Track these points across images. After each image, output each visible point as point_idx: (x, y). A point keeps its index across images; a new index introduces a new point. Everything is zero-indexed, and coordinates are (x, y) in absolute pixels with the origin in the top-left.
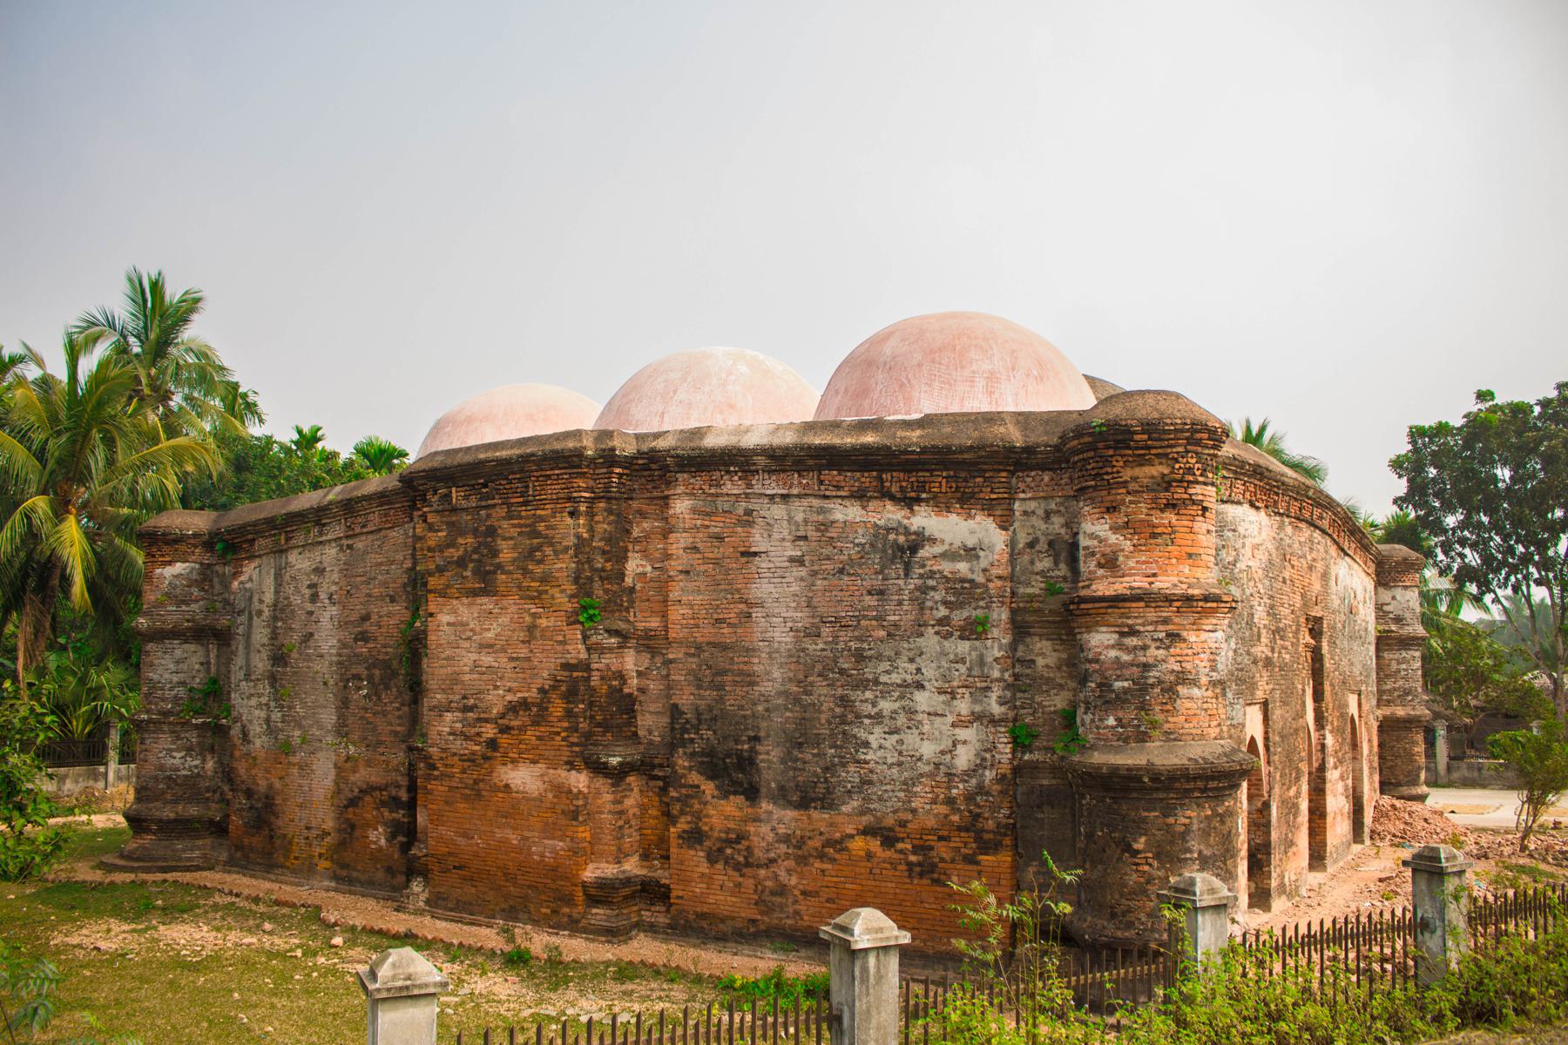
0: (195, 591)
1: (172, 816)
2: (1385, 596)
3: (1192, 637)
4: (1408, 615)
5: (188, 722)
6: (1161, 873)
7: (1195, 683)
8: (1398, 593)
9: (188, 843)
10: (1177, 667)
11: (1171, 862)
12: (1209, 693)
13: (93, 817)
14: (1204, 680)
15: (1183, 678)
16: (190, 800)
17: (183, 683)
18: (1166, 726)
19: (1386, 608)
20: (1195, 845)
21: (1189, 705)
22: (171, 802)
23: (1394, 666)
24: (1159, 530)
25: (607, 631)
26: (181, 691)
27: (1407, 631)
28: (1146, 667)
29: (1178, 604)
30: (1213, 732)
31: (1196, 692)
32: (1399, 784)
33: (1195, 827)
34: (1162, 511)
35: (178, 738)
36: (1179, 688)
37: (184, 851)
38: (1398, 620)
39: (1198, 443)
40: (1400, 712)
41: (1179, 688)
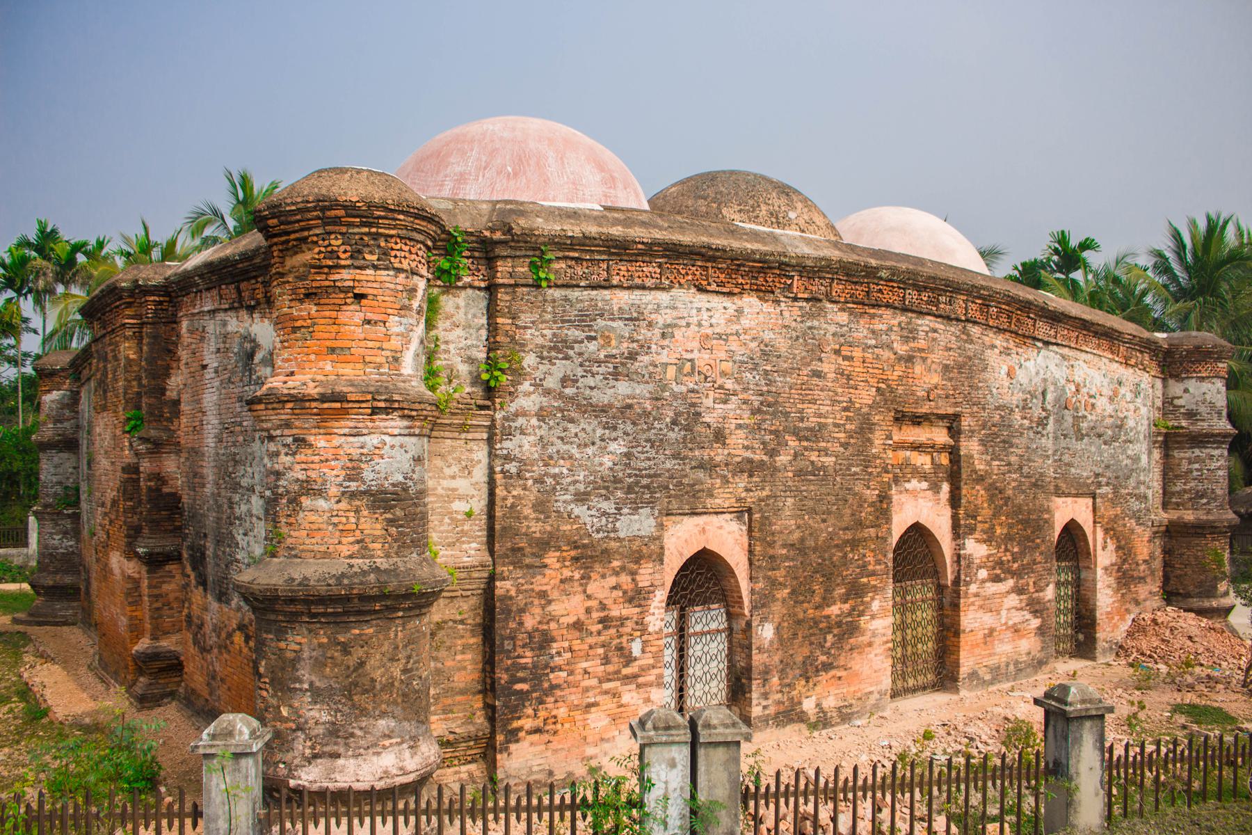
0: (67, 413)
1: (51, 583)
2: (1176, 388)
3: (321, 443)
4: (1203, 409)
5: (60, 513)
6: (274, 702)
7: (320, 493)
8: (1192, 385)
9: (65, 604)
10: (302, 476)
11: (281, 690)
12: (344, 505)
13: (1140, 558)
14: (334, 491)
15: (309, 488)
16: (66, 572)
17: (60, 483)
18: (289, 541)
19: (1177, 402)
20: (306, 674)
21: (314, 518)
22: (53, 573)
23: (1185, 466)
24: (298, 324)
25: (140, 439)
26: (59, 489)
27: (1203, 426)
28: (278, 475)
29: (290, 405)
30: (345, 550)
31: (321, 503)
32: (1188, 595)
33: (306, 655)
34: (301, 301)
35: (57, 525)
36: (303, 499)
37: (60, 610)
38: (1191, 415)
39: (336, 221)
40: (1189, 516)
41: (303, 499)
